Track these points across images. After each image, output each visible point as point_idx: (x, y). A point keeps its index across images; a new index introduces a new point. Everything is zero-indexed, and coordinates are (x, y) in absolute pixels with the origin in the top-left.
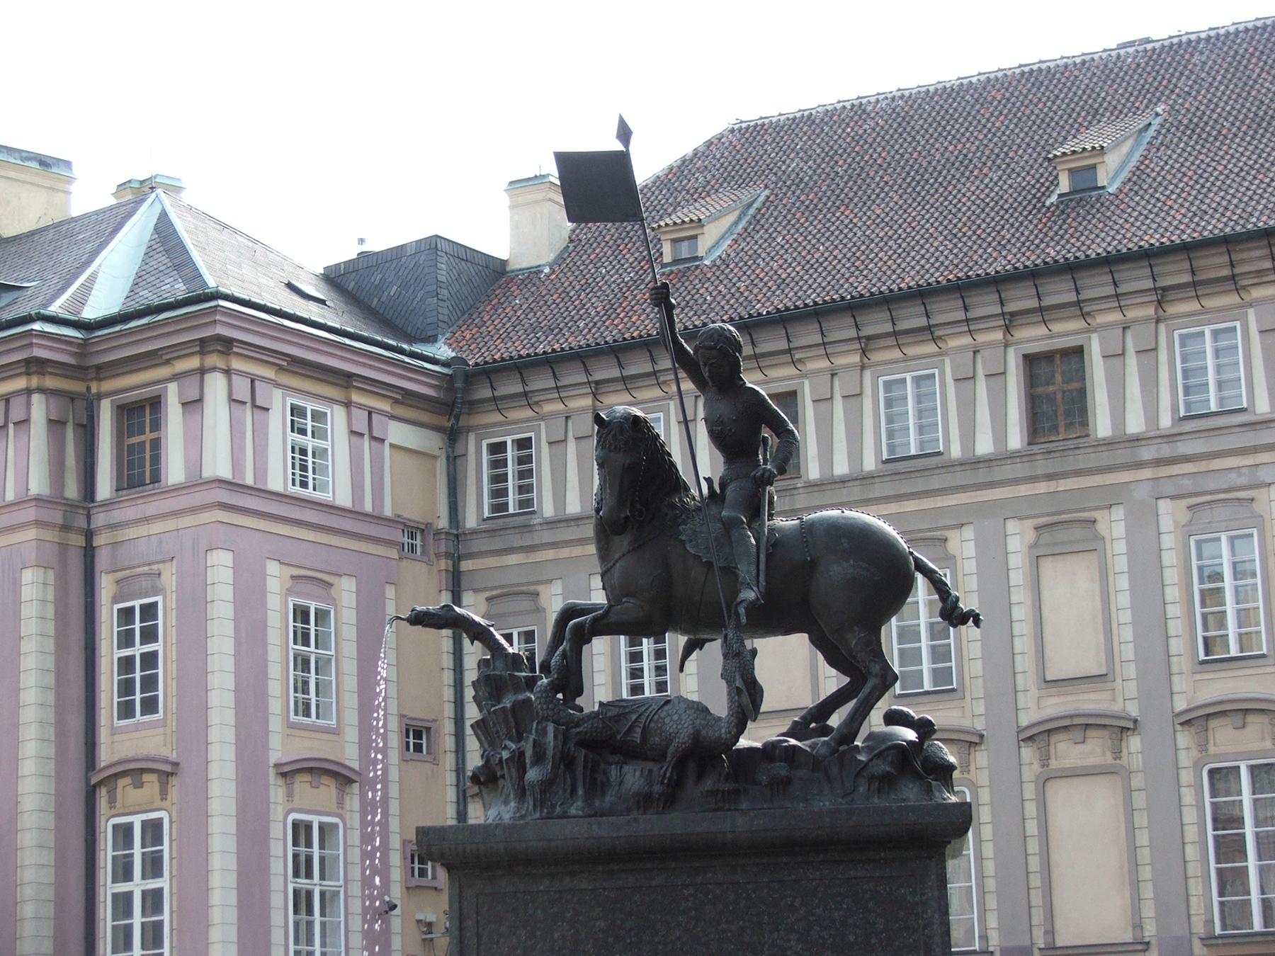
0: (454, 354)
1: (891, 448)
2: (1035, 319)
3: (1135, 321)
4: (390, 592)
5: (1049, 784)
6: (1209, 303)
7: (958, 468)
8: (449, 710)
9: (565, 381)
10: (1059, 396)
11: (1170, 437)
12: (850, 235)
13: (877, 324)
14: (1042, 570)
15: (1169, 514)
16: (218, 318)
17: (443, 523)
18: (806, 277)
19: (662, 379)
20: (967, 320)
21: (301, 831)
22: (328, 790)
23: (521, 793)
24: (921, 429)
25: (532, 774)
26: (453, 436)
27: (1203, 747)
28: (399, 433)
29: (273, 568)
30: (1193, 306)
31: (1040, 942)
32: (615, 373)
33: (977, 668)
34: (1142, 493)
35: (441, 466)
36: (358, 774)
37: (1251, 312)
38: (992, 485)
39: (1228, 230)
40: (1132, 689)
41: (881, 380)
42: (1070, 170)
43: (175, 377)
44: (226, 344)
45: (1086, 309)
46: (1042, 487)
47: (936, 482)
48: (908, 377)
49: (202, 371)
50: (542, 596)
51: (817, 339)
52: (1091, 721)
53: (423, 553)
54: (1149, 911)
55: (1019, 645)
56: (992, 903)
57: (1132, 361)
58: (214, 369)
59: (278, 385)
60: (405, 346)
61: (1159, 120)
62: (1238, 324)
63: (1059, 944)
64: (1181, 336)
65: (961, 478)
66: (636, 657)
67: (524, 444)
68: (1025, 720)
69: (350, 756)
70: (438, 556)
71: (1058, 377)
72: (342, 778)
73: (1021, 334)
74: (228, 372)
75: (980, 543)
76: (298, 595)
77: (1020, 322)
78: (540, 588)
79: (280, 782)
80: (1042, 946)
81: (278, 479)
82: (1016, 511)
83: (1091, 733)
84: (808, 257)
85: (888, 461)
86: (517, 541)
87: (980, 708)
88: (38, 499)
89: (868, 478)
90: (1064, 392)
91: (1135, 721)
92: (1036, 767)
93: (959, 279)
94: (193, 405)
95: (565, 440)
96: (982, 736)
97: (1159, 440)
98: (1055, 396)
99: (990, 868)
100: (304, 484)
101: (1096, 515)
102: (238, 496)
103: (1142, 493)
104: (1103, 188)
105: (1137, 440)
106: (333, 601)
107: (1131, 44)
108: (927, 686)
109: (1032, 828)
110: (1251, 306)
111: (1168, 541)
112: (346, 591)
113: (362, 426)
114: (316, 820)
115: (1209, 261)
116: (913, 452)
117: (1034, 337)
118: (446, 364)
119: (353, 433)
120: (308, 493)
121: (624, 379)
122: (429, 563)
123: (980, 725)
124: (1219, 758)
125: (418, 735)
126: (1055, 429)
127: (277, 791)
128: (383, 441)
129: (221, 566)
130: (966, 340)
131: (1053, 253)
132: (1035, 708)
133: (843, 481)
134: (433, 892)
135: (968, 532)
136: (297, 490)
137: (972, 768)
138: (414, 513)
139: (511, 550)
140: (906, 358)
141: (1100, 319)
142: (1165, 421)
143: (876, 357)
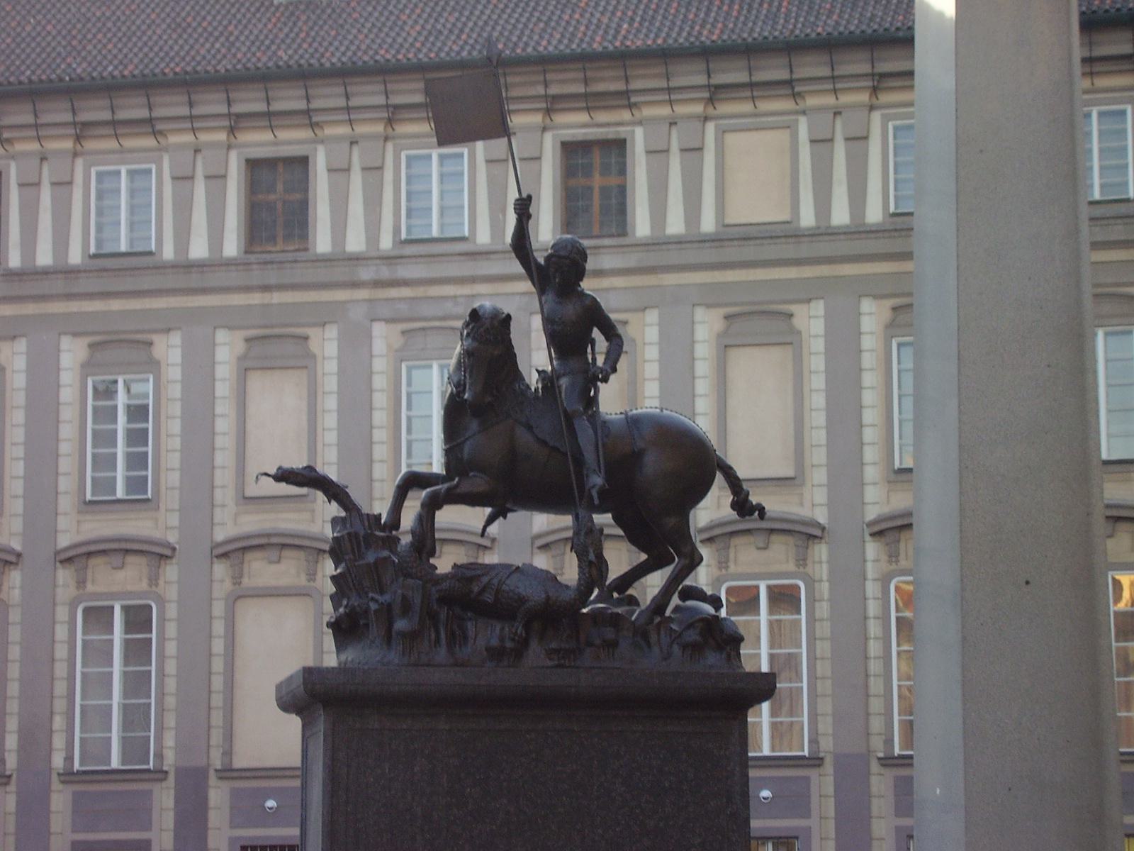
1: (99, 243)
2: (262, 124)
5: (239, 604)
7: (674, 246)
9: (45, 118)
10: (279, 205)
11: (388, 259)
12: (64, 10)
13: (95, 110)
14: (249, 383)
15: (383, 338)
18: (18, 51)
19: (797, 89)
20: (833, 77)
23: (388, 638)
24: (132, 226)
25: (401, 625)
27: (81, 583)
30: (112, 144)
31: (217, 763)
32: (825, 71)
33: (174, 478)
34: (357, 313)
38: (205, 291)
39: (464, 54)
41: (403, 155)
45: (314, 119)
46: (256, 298)
47: (146, 282)
51: (29, 119)
52: (93, 548)
55: (219, 459)
56: (170, 720)
57: (356, 178)
62: (154, 167)
63: (296, 761)
65: (843, 247)
66: (656, 408)
68: (220, 536)
71: (280, 187)
73: (246, 137)
75: (187, 349)
77: (723, 96)
80: (219, 767)
83: (287, 553)
84: (19, 29)
85: (95, 256)
87: (174, 520)
89: (70, 272)
90: (284, 202)
91: (823, 529)
92: (228, 585)
93: (186, 73)
96: (174, 549)
97: (378, 262)
98: (277, 207)
99: (171, 685)
101: (793, 308)
103: (357, 313)
105: (356, 259)
108: (120, 493)
109: (218, 646)
110: (322, 142)
111: (379, 364)
117: (259, 142)
123: (172, 538)
126: (273, 239)
130: (188, 138)
131: (285, 58)
133: (45, 272)
137: (161, 582)
140: (122, 150)
141: (329, 131)
142: (386, 243)
143: (90, 145)
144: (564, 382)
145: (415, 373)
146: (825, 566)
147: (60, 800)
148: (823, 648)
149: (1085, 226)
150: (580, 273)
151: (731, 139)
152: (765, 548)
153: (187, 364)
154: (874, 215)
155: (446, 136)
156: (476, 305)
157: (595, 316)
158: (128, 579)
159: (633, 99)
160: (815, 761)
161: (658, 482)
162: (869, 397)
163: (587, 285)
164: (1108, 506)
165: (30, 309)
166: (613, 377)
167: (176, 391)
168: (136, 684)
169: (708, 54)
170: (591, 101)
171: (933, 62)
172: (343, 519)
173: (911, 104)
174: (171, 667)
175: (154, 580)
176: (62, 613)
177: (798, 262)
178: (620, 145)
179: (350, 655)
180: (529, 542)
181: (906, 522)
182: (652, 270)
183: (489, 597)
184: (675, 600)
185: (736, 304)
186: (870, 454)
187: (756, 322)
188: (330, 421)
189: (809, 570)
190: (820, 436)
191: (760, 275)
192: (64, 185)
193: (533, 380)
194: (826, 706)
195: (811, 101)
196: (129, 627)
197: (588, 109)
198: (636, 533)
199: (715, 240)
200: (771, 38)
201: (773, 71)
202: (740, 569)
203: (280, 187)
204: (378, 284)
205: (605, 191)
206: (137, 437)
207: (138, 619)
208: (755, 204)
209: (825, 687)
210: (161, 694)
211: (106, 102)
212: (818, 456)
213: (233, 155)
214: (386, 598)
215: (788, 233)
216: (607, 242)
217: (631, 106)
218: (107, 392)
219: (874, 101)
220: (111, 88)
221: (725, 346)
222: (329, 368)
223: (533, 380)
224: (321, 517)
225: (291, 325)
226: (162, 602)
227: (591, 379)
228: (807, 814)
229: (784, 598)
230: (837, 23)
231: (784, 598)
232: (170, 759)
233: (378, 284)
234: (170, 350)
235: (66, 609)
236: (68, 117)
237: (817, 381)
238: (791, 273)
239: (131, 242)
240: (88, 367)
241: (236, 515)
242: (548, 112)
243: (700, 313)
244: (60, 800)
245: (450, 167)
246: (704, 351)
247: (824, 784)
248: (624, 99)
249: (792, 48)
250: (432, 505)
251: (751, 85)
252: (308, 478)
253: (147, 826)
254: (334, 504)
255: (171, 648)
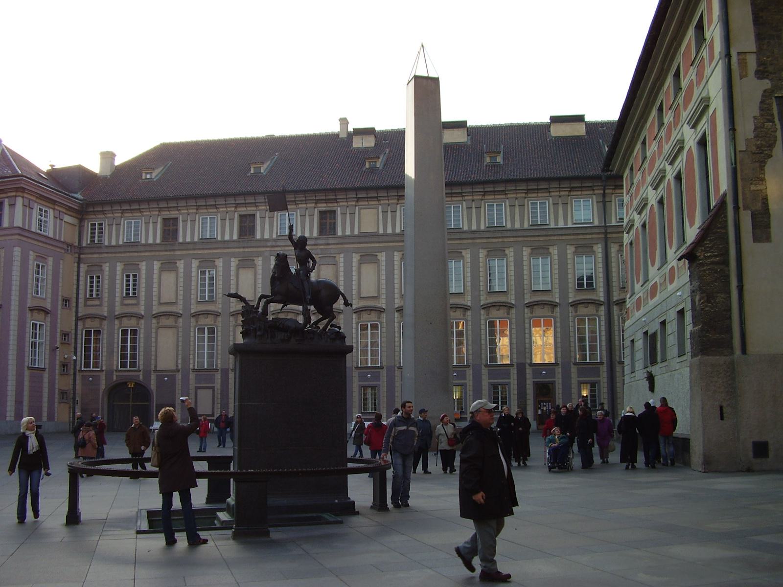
0: (83, 198)
3: (116, 217)
4: (61, 262)
6: (540, 195)
8: (75, 295)
11: (274, 240)
13: (201, 202)
16: (22, 182)
17: (76, 244)
21: (35, 325)
22: (42, 315)
25: (258, 333)
26: (81, 220)
28: (67, 218)
29: (31, 253)
32: (156, 206)
35: (77, 228)
36: (50, 311)
37: (298, 210)
38: (228, 248)
40: (181, 307)
42: (254, 167)
43: (7, 197)
44: (23, 190)
46: (241, 250)
47: (505, 234)
48: (133, 221)
49: (16, 196)
50: (103, 267)
53: (71, 251)
54: (180, 361)
56: (219, 357)
57: (267, 219)
58: (19, 196)
59: (36, 202)
60: (70, 194)
61: (276, 157)
62: (295, 213)
63: (158, 369)
64: (202, 218)
67: (101, 224)
69: (48, 306)
70: (75, 253)
71: (248, 222)
72: (46, 312)
74: (23, 197)
75: (147, 266)
76: (37, 261)
78: (103, 264)
79: (30, 312)
81: (34, 228)
82: (356, 251)
85: (201, 239)
86: (97, 251)
88: (87, 219)
89: (195, 243)
91: (342, 311)
94: (12, 205)
95: (113, 225)
98: (170, 230)
99: (220, 348)
100: (41, 231)
102: (23, 232)
104: (262, 173)
105: (267, 240)
106: (47, 263)
107: (268, 136)
108: (207, 299)
110: (258, 210)
112: (50, 261)
113: (57, 215)
114: (38, 323)
115: (290, 196)
116: (208, 237)
117: (243, 210)
118: (81, 200)
119: (55, 217)
120: (42, 232)
121: (168, 207)
122: (72, 255)
123: (220, 311)
124: (201, 325)
125: (66, 302)
126: (246, 235)
127: (29, 315)
128: (62, 220)
129: (17, 251)
132: (156, 309)
133: (188, 243)
134: (68, 345)
135: (221, 260)
136: (38, 231)
137: (217, 322)
138: (69, 241)
139: (95, 253)
142: (274, 236)
144: (301, 272)
145: (490, 261)
146: (385, 319)
147: (192, 376)
148: (384, 339)
149: (446, 235)
150: (306, 245)
151: (362, 211)
152: (370, 314)
153: (185, 268)
154: (398, 231)
155: (273, 209)
156: (279, 252)
157: (309, 255)
158: (208, 321)
159: (338, 201)
160: (468, 366)
161: (325, 297)
162: (396, 276)
163: (308, 248)
164: (451, 305)
165: (184, 252)
166: (313, 271)
167: (221, 273)
168: (211, 348)
169: (356, 190)
170: (327, 201)
171: (409, 191)
172: (244, 306)
173: (404, 203)
174: (220, 343)
175: (215, 321)
176: (192, 330)
177: (379, 242)
178: (334, 212)
179: (246, 340)
180: (294, 312)
181: (624, 301)
182: (342, 244)
183: (281, 326)
184: (329, 327)
185: (490, 248)
186: (396, 291)
187: (369, 257)
188: (383, 277)
189: (466, 317)
190: (384, 286)
191: (369, 246)
192: (118, 225)
193: (293, 271)
194: (384, 354)
195: (509, 196)
196: (209, 333)
197: (326, 203)
198: (320, 310)
199: (358, 236)
200: (479, 180)
201: (373, 194)
202: (201, 323)
203: (248, 222)
204: (272, 246)
205: (330, 224)
206: (211, 285)
207: (211, 331)
208: (368, 227)
209: (384, 349)
210: (217, 350)
211: (396, 191)
212: (181, 297)
213: (236, 213)
214: (254, 327)
215: (376, 235)
216: (331, 236)
217: (337, 202)
218: (203, 273)
219: (197, 212)
220: (205, 197)
221: (360, 263)
222: (181, 270)
223: (293, 271)
224: (236, 306)
225: (250, 257)
226: (217, 327)
227: (309, 271)
228: (379, 381)
229: (374, 327)
230: (389, 183)
231: (374, 327)
232: (219, 366)
233: (272, 246)
234: (219, 263)
235: (484, 321)
236: (157, 206)
237: (383, 272)
238: (377, 245)
239: (210, 236)
240: (199, 267)
241: (236, 305)
242: (316, 203)
243: (354, 255)
244: (192, 376)
245: (587, 203)
246: (156, 272)
247: (384, 373)
248: (335, 201)
249: (377, 189)
250: (267, 303)
251: (494, 191)
252: (236, 296)
253: (214, 383)
254: (243, 303)
255: (220, 338)
